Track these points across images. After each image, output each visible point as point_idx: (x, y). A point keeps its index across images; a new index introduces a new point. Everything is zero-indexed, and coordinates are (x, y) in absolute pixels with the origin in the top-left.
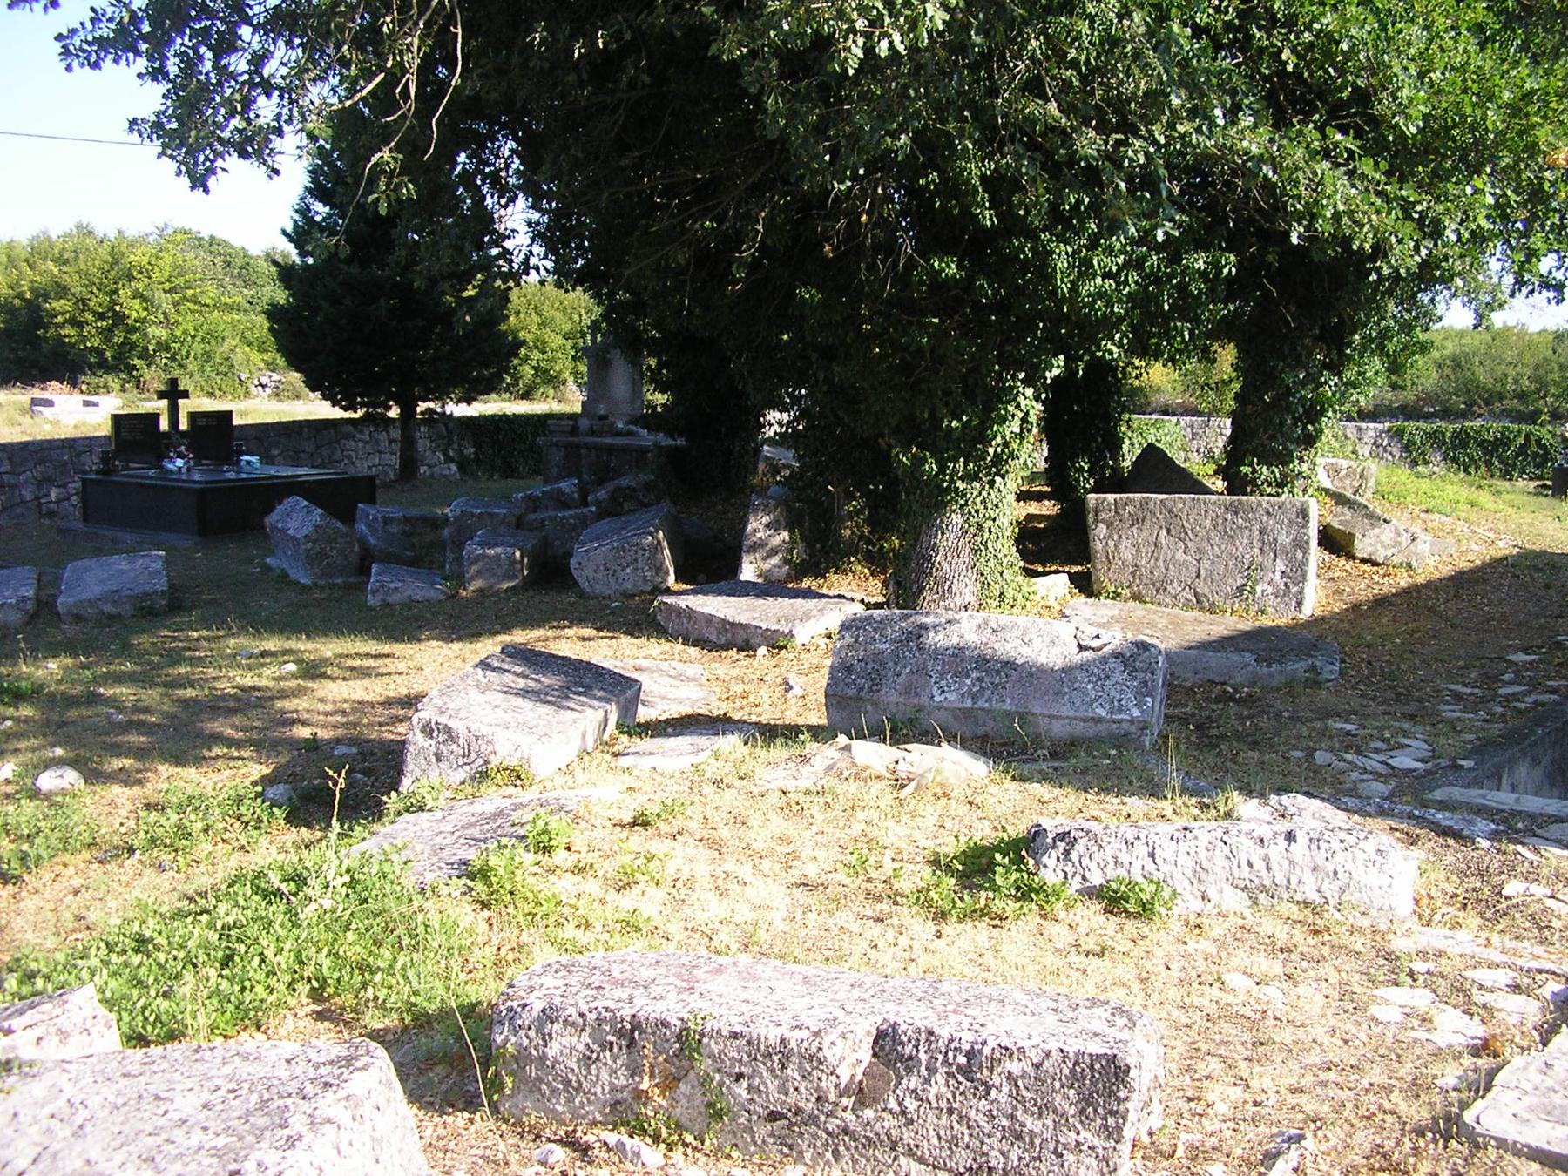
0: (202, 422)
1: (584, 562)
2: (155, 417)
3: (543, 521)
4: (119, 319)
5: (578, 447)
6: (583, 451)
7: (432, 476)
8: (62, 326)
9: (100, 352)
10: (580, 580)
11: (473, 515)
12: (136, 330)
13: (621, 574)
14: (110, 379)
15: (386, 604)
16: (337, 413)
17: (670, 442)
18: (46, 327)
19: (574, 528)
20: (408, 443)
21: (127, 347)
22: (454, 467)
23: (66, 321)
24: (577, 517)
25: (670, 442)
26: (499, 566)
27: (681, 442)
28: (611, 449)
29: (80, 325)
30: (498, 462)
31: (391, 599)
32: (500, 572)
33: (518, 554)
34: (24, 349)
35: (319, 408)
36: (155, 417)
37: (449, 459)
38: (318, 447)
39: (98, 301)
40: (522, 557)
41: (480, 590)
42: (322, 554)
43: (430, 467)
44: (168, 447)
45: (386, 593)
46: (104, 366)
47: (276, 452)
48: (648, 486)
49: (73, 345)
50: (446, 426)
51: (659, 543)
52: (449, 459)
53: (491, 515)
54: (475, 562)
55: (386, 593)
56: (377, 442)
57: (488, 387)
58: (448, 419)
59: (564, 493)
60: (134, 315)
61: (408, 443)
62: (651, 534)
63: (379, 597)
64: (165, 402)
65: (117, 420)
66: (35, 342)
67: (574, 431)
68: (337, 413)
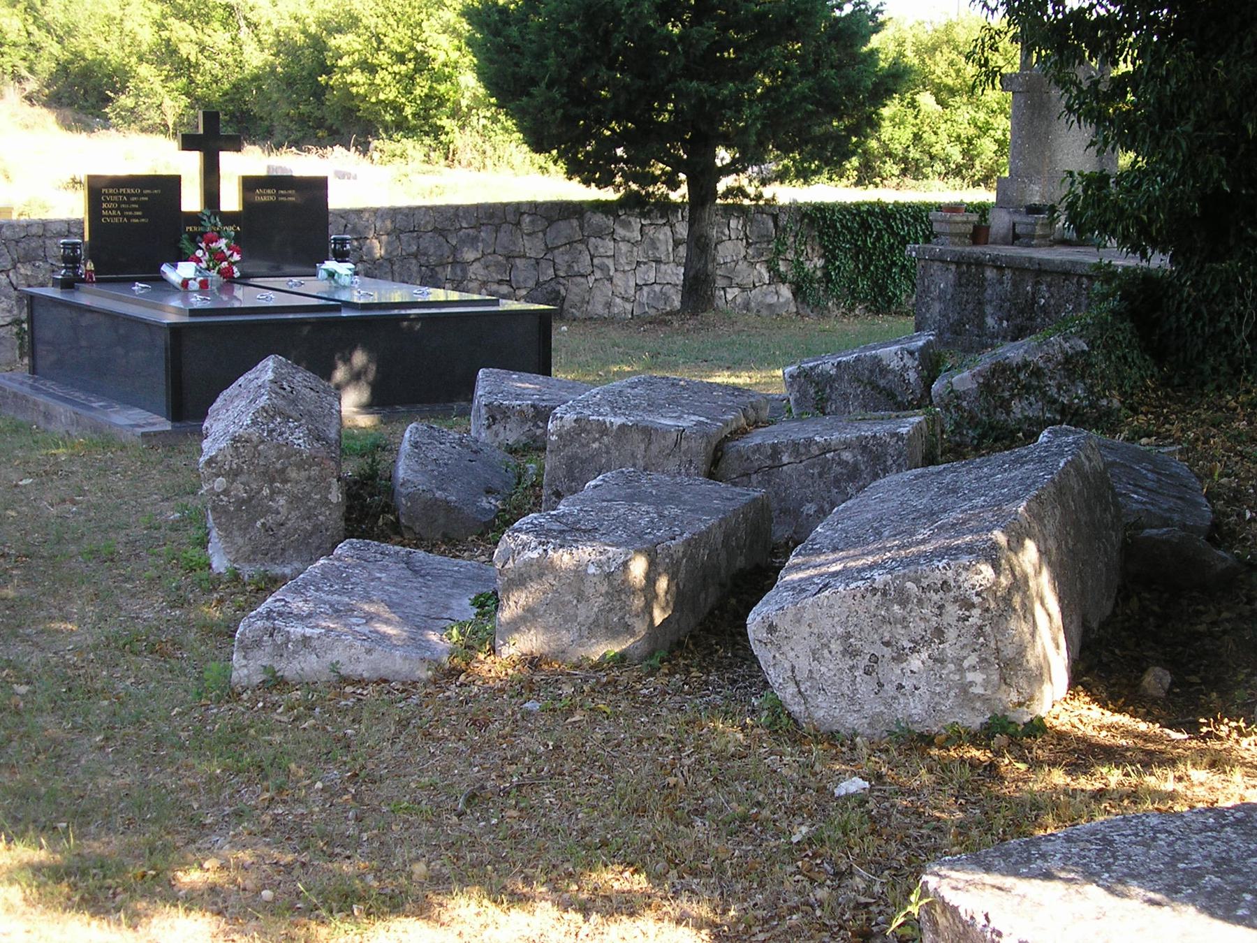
0: (265, 196)
1: (783, 624)
2: (173, 183)
3: (776, 451)
4: (422, 61)
5: (980, 263)
6: (990, 274)
7: (747, 306)
8: (346, 70)
9: (398, 109)
10: (772, 675)
11: (603, 429)
12: (448, 78)
13: (893, 673)
14: (409, 144)
15: (275, 682)
16: (578, 192)
17: (1133, 261)
18: (329, 71)
19: (853, 474)
20: (699, 247)
21: (433, 102)
22: (786, 291)
23: (355, 64)
24: (863, 446)
25: (1133, 261)
26: (580, 596)
27: (1159, 261)
28: (1041, 271)
29: (372, 69)
30: (863, 284)
31: (290, 668)
32: (585, 612)
33: (639, 568)
34: (307, 102)
35: (549, 183)
36: (173, 183)
37: (777, 277)
38: (549, 250)
39: (396, 38)
40: (651, 578)
41: (533, 662)
42: (250, 506)
43: (743, 288)
44: (193, 239)
45: (279, 651)
46: (401, 126)
47: (469, 255)
48: (1072, 366)
49: (364, 98)
50: (775, 218)
51: (1020, 584)
52: (777, 277)
53: (648, 432)
54: (519, 581)
55: (279, 651)
56: (653, 244)
57: (829, 155)
58: (771, 210)
59: (884, 371)
60: (441, 58)
61: (699, 247)
62: (992, 555)
63: (262, 658)
64: (195, 158)
65: (100, 191)
66: (320, 92)
67: (979, 234)
68: (578, 192)
